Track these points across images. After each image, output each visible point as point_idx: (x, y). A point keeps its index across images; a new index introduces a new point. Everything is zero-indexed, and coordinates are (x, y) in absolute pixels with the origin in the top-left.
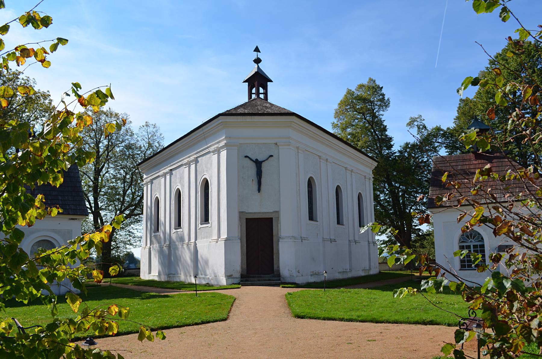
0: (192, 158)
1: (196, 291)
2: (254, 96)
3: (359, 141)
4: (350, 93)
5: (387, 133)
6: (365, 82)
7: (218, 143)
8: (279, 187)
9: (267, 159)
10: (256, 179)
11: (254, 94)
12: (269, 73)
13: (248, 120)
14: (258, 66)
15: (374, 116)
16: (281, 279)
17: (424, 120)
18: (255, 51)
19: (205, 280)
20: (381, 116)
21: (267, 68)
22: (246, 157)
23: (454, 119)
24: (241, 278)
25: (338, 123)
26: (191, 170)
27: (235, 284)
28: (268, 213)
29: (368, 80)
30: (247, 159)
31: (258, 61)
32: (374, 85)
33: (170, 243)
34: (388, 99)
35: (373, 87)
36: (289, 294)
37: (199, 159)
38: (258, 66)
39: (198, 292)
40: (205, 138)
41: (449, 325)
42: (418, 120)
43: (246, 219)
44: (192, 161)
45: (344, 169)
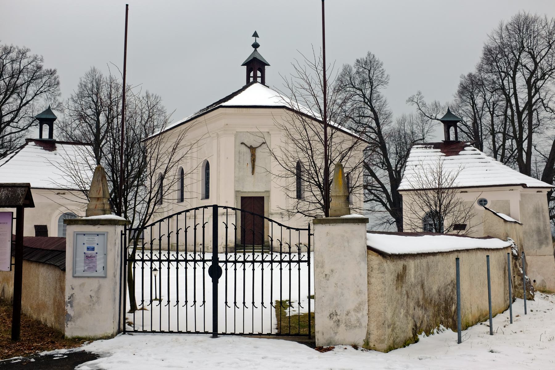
9: (260, 146)
12: (267, 59)
18: (253, 36)
21: (264, 53)
22: (242, 143)
28: (260, 192)
30: (243, 145)
31: (256, 46)
41: (506, 310)
43: (242, 197)
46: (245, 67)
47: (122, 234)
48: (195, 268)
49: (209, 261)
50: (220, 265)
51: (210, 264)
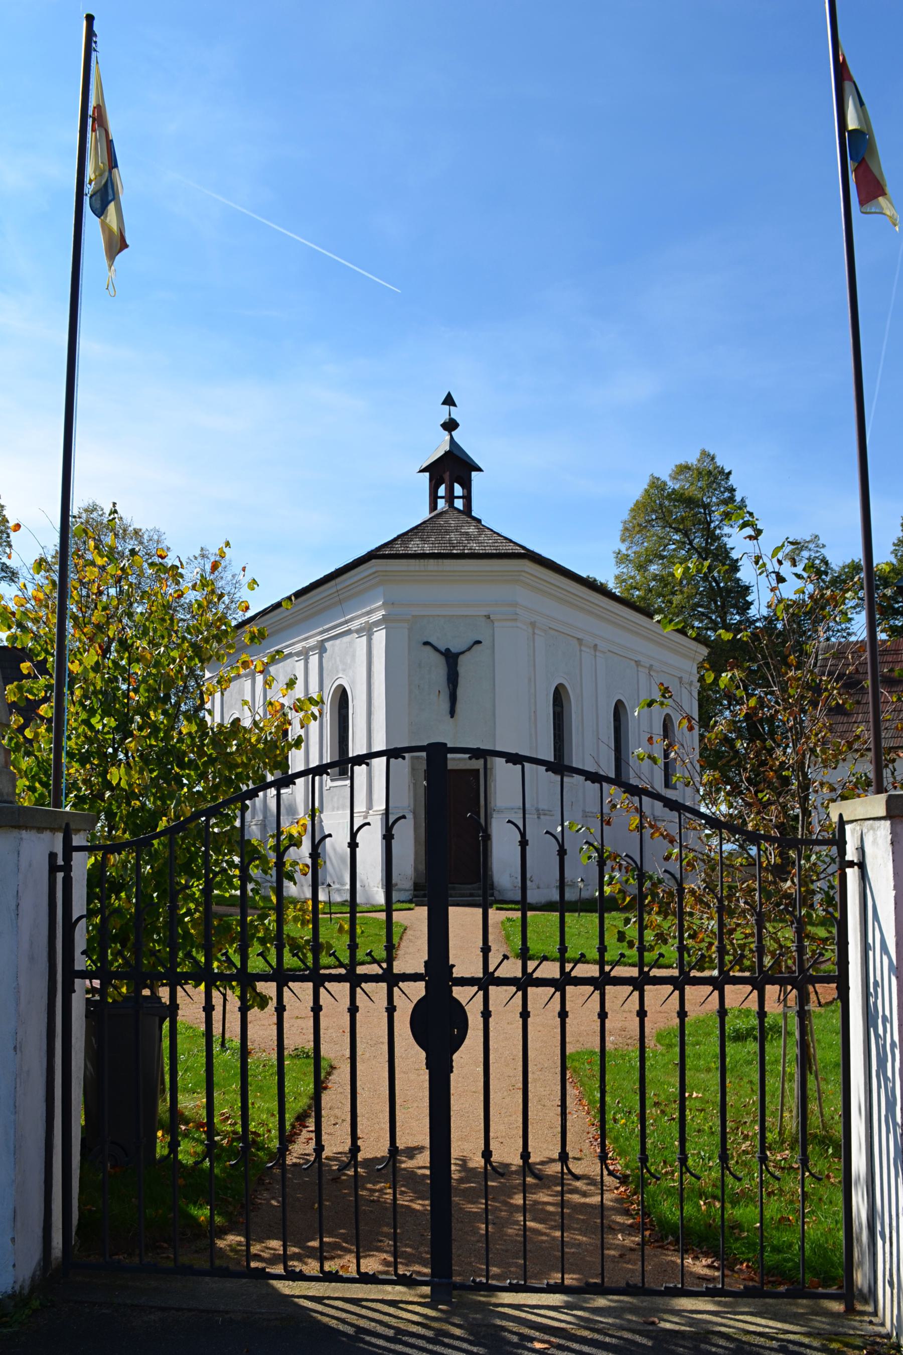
0: (312, 642)
1: (331, 913)
2: (441, 504)
3: (673, 593)
4: (656, 485)
5: (738, 575)
6: (692, 459)
7: (368, 613)
8: (494, 706)
9: (469, 649)
10: (447, 690)
11: (442, 497)
13: (430, 568)
14: (452, 437)
15: (711, 536)
16: (496, 893)
17: (824, 546)
18: (444, 403)
19: (340, 895)
20: (725, 539)
21: (469, 442)
22: (426, 643)
23: (894, 545)
24: (415, 890)
25: (629, 552)
26: (310, 665)
27: (403, 902)
29: (698, 455)
30: (428, 648)
31: (450, 426)
32: (711, 468)
33: (265, 817)
34: (743, 500)
35: (710, 473)
36: (509, 920)
37: (327, 645)
38: (452, 437)
39: (333, 916)
40: (340, 602)
42: (812, 546)
44: (312, 648)
45: (633, 663)
46: (427, 475)
47: (53, 868)
48: (353, 1010)
49: (415, 977)
50: (459, 993)
51: (418, 990)
